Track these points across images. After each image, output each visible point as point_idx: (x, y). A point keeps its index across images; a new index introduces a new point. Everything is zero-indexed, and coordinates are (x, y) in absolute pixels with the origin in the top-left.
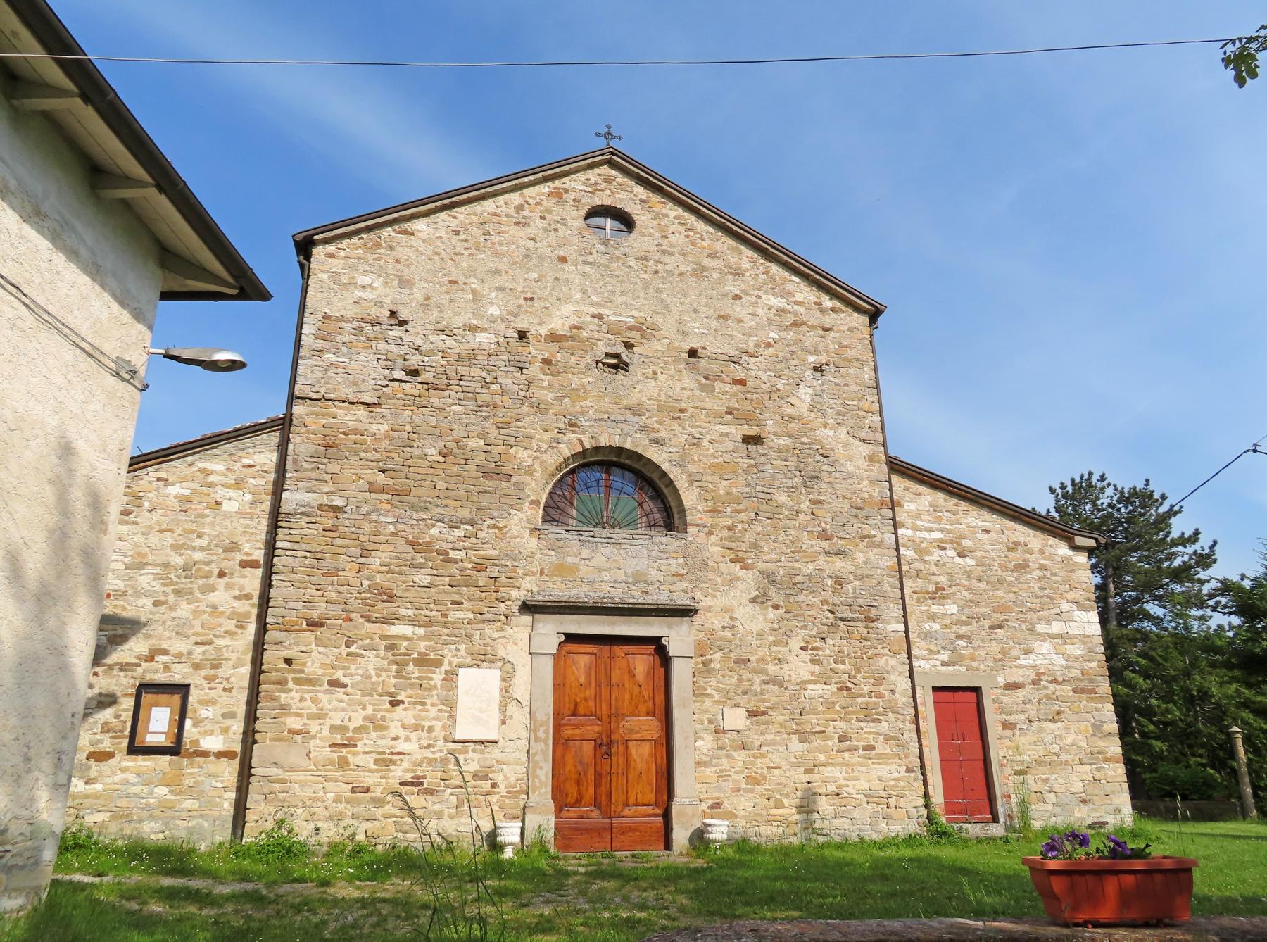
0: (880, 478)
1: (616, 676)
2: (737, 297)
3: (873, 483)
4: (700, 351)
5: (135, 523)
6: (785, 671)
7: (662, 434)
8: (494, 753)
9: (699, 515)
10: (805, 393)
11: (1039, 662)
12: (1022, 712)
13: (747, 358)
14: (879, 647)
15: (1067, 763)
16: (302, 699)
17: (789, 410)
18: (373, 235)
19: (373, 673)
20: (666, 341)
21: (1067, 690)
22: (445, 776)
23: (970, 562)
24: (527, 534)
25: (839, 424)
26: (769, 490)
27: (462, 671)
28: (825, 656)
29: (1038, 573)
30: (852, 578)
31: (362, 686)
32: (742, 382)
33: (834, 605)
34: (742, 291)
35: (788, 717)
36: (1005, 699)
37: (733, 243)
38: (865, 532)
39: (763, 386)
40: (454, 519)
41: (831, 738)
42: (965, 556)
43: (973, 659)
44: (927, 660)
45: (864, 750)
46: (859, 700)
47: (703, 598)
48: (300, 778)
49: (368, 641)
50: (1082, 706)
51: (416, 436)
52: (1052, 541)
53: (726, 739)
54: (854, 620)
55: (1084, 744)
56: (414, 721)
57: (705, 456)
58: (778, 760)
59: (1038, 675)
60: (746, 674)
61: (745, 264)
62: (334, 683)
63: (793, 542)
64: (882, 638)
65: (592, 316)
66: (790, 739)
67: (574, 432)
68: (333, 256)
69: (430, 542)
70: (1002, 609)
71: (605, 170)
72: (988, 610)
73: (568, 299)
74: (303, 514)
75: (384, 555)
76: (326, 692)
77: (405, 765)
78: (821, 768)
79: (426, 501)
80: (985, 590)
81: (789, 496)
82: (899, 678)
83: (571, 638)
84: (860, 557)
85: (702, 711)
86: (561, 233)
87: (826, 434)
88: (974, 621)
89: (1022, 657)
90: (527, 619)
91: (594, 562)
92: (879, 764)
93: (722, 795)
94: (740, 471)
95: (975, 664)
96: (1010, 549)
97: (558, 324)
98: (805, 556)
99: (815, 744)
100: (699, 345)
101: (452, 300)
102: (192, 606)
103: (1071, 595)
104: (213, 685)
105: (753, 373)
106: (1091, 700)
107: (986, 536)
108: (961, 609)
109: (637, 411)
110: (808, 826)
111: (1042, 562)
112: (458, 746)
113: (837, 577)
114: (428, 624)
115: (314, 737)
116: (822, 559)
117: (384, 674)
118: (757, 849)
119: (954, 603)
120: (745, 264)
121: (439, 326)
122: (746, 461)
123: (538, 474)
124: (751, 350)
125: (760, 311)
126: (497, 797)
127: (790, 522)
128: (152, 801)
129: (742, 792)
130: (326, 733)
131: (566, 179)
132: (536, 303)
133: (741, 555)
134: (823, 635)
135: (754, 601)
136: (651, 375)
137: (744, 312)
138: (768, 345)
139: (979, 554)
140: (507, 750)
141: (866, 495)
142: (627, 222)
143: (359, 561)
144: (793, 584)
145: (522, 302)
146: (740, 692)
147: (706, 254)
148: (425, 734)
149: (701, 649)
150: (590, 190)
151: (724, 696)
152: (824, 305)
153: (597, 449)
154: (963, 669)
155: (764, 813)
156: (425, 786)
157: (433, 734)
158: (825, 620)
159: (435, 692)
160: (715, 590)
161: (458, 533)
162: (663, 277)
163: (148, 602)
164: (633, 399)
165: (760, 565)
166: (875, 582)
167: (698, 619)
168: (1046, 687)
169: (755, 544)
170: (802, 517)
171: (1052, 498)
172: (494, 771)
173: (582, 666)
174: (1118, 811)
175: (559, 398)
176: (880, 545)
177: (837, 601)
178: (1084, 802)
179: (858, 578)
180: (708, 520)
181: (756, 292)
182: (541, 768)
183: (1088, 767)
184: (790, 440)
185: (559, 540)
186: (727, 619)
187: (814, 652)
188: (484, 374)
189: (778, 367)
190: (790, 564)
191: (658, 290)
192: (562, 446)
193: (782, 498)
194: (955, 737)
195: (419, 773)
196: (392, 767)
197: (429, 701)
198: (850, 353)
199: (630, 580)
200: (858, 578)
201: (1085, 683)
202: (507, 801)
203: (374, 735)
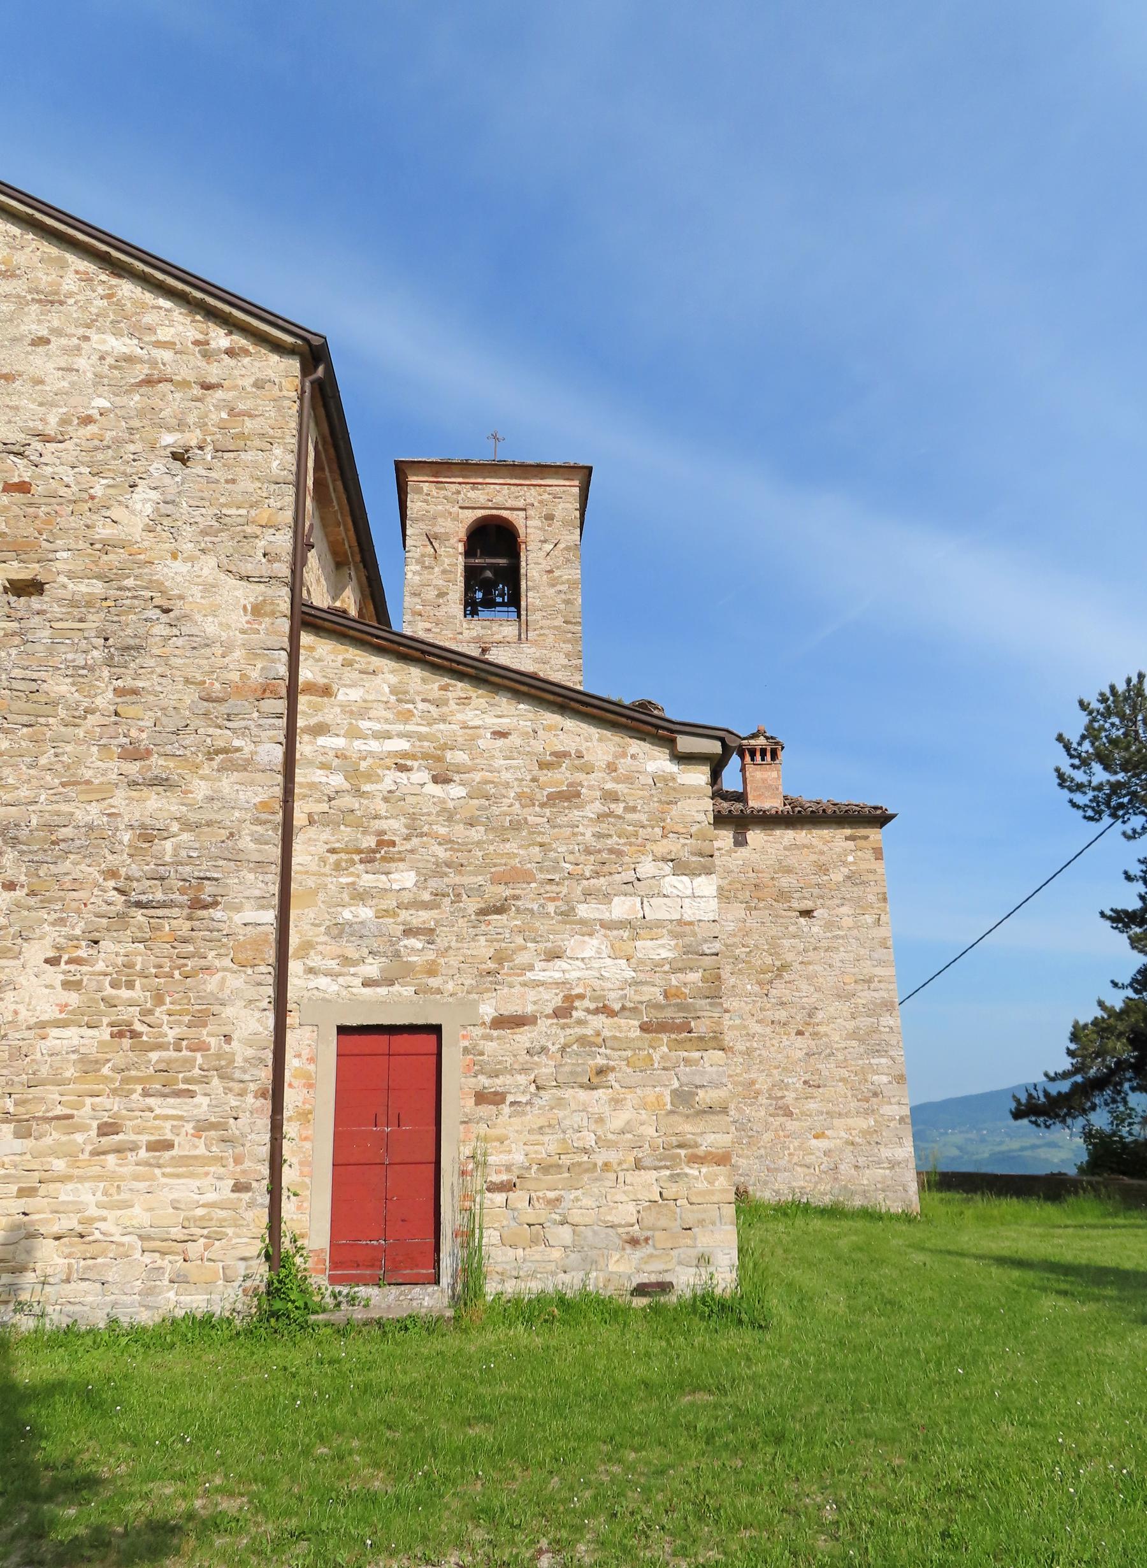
2: (43, 341)
3: (252, 653)
10: (144, 501)
11: (573, 975)
12: (524, 1070)
13: (39, 446)
15: (607, 1166)
17: (104, 531)
21: (630, 1027)
23: (456, 791)
25: (203, 551)
26: (35, 676)
28: (93, 974)
29: (598, 807)
30: (175, 827)
32: (23, 487)
33: (128, 878)
34: (53, 331)
36: (490, 1047)
37: (53, 250)
38: (221, 744)
39: (63, 491)
41: (82, 1128)
42: (447, 781)
43: (432, 971)
45: (148, 1149)
46: (154, 1056)
50: (656, 1057)
52: (636, 746)
54: (163, 905)
55: (650, 1131)
59: (569, 999)
61: (70, 283)
70: (513, 876)
72: (480, 879)
78: (52, 1186)
80: (479, 843)
81: (73, 684)
84: (200, 789)
88: (446, 901)
89: (539, 965)
92: (178, 1176)
95: (434, 982)
96: (542, 765)
98: (87, 792)
99: (48, 1141)
103: (662, 848)
105: (48, 470)
106: (677, 1045)
107: (501, 742)
111: (609, 786)
113: (143, 826)
116: (120, 799)
119: (411, 868)
120: (70, 283)
124: (51, 429)
125: (82, 363)
127: (71, 729)
134: (96, 935)
137: (50, 366)
138: (87, 420)
139: (477, 777)
141: (235, 676)
144: (53, 843)
152: (213, 345)
158: (105, 907)
168: (581, 1022)
171: (1084, 719)
174: (704, 1260)
176: (246, 766)
177: (135, 870)
178: (634, 1242)
179: (187, 826)
181: (81, 331)
183: (654, 1174)
187: (72, 967)
189: (100, 456)
190: (55, 807)
194: (382, 1119)
198: (249, 425)
200: (187, 826)
201: (669, 1013)
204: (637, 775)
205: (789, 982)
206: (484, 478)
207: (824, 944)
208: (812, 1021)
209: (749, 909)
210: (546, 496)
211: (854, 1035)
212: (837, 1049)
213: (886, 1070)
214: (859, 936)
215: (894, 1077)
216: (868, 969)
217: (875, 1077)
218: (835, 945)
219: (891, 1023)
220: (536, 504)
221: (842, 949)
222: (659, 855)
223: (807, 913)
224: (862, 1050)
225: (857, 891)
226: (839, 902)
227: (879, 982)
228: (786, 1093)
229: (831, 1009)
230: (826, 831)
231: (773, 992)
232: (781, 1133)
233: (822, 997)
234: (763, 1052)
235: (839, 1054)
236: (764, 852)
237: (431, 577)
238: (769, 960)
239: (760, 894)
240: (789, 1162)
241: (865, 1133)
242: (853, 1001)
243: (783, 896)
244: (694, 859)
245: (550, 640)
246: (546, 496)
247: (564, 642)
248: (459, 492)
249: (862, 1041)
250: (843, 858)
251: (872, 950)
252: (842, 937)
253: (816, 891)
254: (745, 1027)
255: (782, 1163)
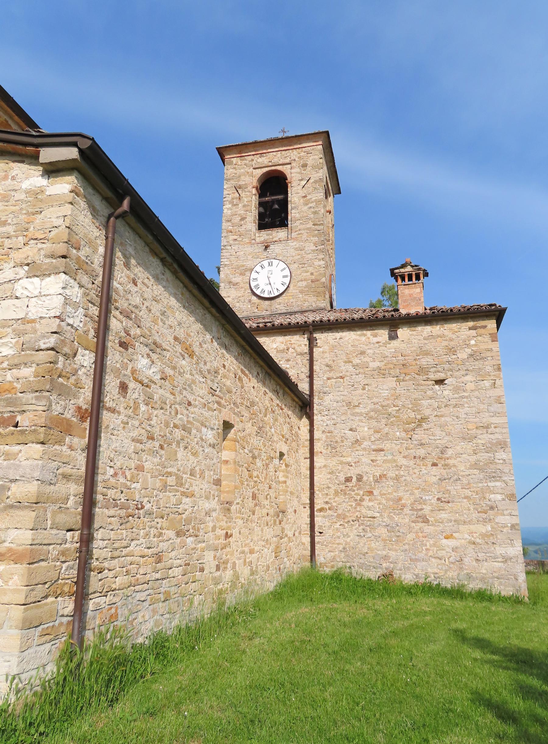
204: (13, 193)
205: (427, 430)
206: (267, 149)
207: (453, 402)
208: (444, 456)
209: (398, 381)
210: (303, 154)
211: (475, 466)
212: (463, 476)
213: (500, 491)
214: (479, 395)
215: (507, 496)
216: (486, 418)
217: (492, 496)
218: (461, 403)
219: (504, 456)
220: (297, 159)
221: (466, 405)
222: (18, 261)
223: (440, 382)
224: (481, 476)
225: (478, 364)
226: (464, 373)
227: (495, 427)
228: (424, 507)
229: (458, 448)
230: (454, 325)
231: (415, 436)
232: (420, 534)
233: (451, 439)
234: (408, 478)
235: (464, 479)
236: (409, 342)
237: (237, 210)
238: (412, 415)
239: (406, 371)
240: (426, 555)
241: (483, 536)
242: (474, 441)
243: (422, 370)
244: (48, 260)
245: (305, 236)
246: (303, 154)
247: (313, 236)
248: (253, 160)
249: (481, 470)
250: (467, 342)
251: (490, 405)
252: (467, 397)
253: (447, 366)
254: (395, 461)
255: (421, 555)
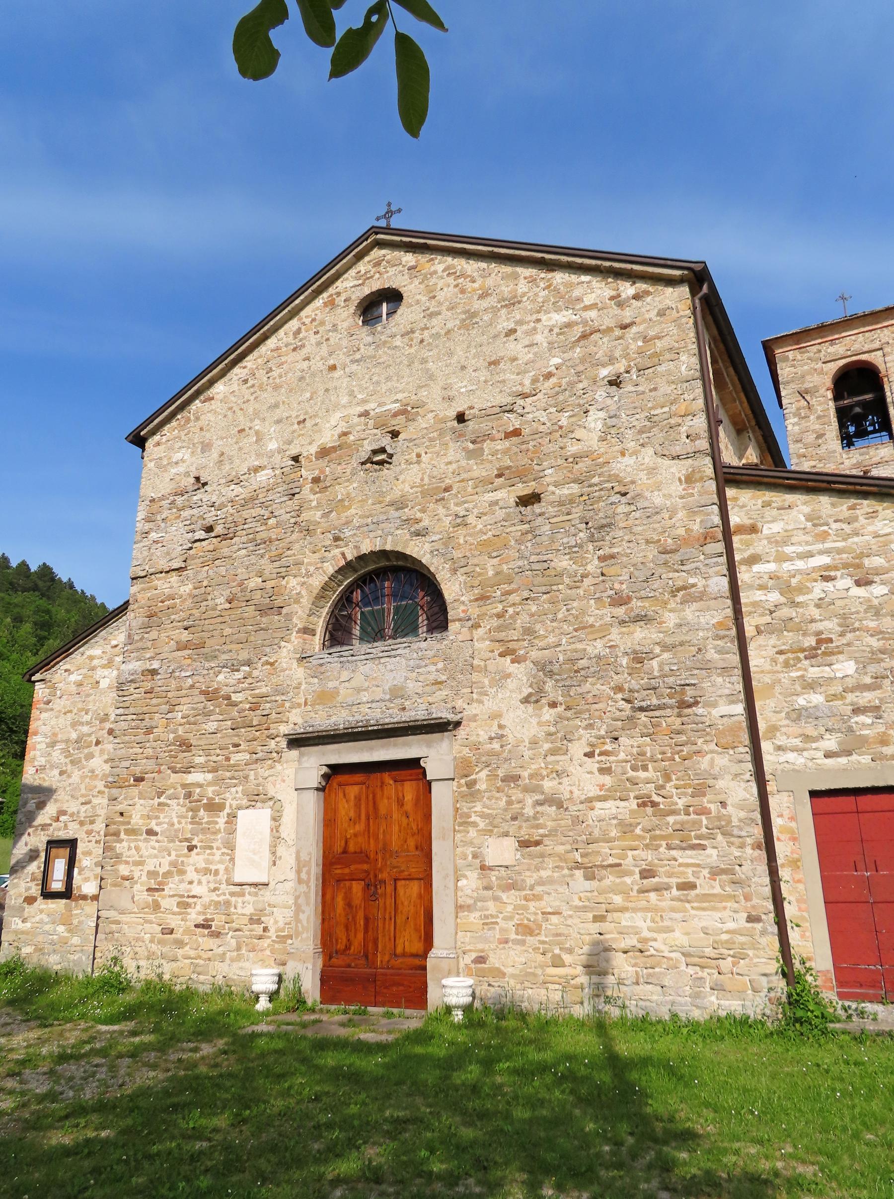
0: (703, 503)
1: (383, 806)
3: (692, 512)
4: (467, 412)
5: (52, 710)
6: (564, 788)
7: (425, 523)
8: (266, 895)
9: (462, 608)
10: (595, 420)
14: (700, 741)
16: (129, 849)
17: (573, 449)
18: (185, 413)
19: (175, 820)
20: (431, 415)
22: (228, 919)
24: (295, 664)
25: (642, 445)
27: (240, 813)
28: (618, 762)
30: (657, 650)
31: (168, 833)
32: (516, 433)
33: (630, 691)
35: (568, 847)
38: (680, 583)
39: (542, 428)
40: (235, 662)
41: (629, 873)
42: (869, 583)
44: (799, 750)
46: (671, 819)
47: (466, 706)
48: (128, 920)
49: (172, 791)
51: (210, 589)
53: (493, 876)
54: (659, 708)
56: (204, 865)
57: (471, 535)
58: (557, 903)
60: (516, 794)
61: (522, 287)
62: (151, 832)
63: (576, 617)
64: (704, 729)
65: (359, 416)
66: (572, 876)
67: (337, 547)
68: (158, 444)
69: (217, 689)
71: (376, 253)
73: (336, 406)
74: (131, 681)
75: (185, 707)
76: (145, 840)
77: (199, 908)
78: (615, 915)
79: (215, 650)
81: (571, 559)
82: (732, 784)
83: (335, 770)
84: (671, 619)
85: (465, 843)
86: (332, 341)
87: (624, 466)
90: (294, 753)
91: (353, 683)
92: (704, 909)
93: (487, 947)
94: (513, 543)
97: (328, 438)
98: (592, 633)
99: (607, 882)
100: (466, 406)
101: (240, 449)
102: (80, 773)
104: (90, 838)
105: (530, 416)
108: (863, 666)
109: (399, 504)
110: (598, 991)
112: (237, 889)
113: (635, 652)
114: (214, 770)
115: (136, 882)
116: (615, 634)
117: (183, 821)
118: (523, 1016)
119: (850, 658)
120: (522, 287)
121: (230, 478)
122: (519, 528)
123: (304, 601)
125: (539, 338)
126: (268, 941)
127: (574, 591)
128: (55, 937)
129: (510, 944)
130: (144, 878)
131: (338, 283)
132: (308, 424)
133: (511, 645)
135: (526, 700)
136: (415, 459)
138: (549, 375)
140: (277, 893)
142: (393, 296)
143: (167, 717)
144: (576, 672)
145: (296, 426)
146: (508, 817)
147: (476, 297)
148: (212, 878)
149: (464, 769)
150: (360, 282)
151: (491, 824)
153: (361, 558)
154: (866, 759)
155: (539, 971)
156: (213, 928)
157: (218, 878)
158: (618, 713)
159: (219, 836)
160: (481, 694)
161: (239, 675)
162: (429, 344)
163: (56, 772)
164: (396, 494)
165: (534, 654)
166: (694, 649)
167: (461, 732)
169: (529, 629)
170: (587, 582)
172: (266, 915)
173: (352, 798)
175: (326, 515)
176: (702, 596)
177: (634, 684)
179: (666, 648)
180: (474, 611)
181: (535, 317)
182: (303, 912)
184: (576, 486)
185: (321, 665)
186: (495, 728)
187: (603, 758)
188: (262, 512)
190: (573, 646)
191: (424, 361)
192: (325, 564)
193: (563, 563)
194: (861, 865)
195: (209, 916)
196: (189, 910)
197: (214, 845)
199: (388, 697)
200: (666, 648)
202: (277, 946)
203: (177, 878)
